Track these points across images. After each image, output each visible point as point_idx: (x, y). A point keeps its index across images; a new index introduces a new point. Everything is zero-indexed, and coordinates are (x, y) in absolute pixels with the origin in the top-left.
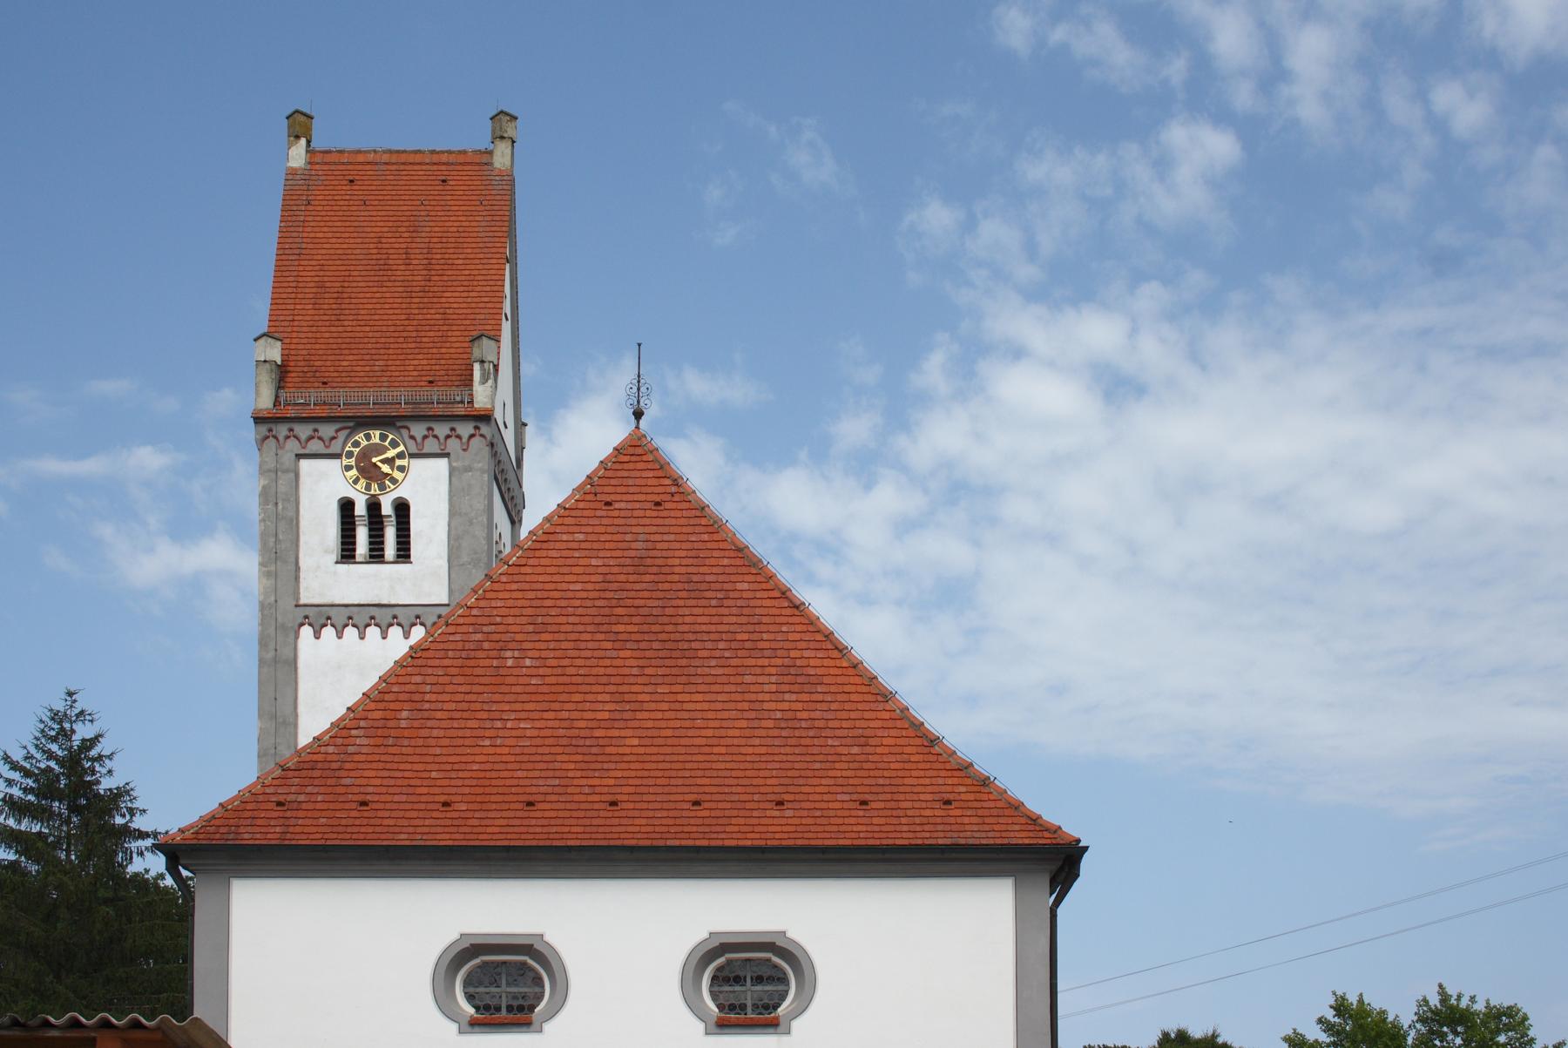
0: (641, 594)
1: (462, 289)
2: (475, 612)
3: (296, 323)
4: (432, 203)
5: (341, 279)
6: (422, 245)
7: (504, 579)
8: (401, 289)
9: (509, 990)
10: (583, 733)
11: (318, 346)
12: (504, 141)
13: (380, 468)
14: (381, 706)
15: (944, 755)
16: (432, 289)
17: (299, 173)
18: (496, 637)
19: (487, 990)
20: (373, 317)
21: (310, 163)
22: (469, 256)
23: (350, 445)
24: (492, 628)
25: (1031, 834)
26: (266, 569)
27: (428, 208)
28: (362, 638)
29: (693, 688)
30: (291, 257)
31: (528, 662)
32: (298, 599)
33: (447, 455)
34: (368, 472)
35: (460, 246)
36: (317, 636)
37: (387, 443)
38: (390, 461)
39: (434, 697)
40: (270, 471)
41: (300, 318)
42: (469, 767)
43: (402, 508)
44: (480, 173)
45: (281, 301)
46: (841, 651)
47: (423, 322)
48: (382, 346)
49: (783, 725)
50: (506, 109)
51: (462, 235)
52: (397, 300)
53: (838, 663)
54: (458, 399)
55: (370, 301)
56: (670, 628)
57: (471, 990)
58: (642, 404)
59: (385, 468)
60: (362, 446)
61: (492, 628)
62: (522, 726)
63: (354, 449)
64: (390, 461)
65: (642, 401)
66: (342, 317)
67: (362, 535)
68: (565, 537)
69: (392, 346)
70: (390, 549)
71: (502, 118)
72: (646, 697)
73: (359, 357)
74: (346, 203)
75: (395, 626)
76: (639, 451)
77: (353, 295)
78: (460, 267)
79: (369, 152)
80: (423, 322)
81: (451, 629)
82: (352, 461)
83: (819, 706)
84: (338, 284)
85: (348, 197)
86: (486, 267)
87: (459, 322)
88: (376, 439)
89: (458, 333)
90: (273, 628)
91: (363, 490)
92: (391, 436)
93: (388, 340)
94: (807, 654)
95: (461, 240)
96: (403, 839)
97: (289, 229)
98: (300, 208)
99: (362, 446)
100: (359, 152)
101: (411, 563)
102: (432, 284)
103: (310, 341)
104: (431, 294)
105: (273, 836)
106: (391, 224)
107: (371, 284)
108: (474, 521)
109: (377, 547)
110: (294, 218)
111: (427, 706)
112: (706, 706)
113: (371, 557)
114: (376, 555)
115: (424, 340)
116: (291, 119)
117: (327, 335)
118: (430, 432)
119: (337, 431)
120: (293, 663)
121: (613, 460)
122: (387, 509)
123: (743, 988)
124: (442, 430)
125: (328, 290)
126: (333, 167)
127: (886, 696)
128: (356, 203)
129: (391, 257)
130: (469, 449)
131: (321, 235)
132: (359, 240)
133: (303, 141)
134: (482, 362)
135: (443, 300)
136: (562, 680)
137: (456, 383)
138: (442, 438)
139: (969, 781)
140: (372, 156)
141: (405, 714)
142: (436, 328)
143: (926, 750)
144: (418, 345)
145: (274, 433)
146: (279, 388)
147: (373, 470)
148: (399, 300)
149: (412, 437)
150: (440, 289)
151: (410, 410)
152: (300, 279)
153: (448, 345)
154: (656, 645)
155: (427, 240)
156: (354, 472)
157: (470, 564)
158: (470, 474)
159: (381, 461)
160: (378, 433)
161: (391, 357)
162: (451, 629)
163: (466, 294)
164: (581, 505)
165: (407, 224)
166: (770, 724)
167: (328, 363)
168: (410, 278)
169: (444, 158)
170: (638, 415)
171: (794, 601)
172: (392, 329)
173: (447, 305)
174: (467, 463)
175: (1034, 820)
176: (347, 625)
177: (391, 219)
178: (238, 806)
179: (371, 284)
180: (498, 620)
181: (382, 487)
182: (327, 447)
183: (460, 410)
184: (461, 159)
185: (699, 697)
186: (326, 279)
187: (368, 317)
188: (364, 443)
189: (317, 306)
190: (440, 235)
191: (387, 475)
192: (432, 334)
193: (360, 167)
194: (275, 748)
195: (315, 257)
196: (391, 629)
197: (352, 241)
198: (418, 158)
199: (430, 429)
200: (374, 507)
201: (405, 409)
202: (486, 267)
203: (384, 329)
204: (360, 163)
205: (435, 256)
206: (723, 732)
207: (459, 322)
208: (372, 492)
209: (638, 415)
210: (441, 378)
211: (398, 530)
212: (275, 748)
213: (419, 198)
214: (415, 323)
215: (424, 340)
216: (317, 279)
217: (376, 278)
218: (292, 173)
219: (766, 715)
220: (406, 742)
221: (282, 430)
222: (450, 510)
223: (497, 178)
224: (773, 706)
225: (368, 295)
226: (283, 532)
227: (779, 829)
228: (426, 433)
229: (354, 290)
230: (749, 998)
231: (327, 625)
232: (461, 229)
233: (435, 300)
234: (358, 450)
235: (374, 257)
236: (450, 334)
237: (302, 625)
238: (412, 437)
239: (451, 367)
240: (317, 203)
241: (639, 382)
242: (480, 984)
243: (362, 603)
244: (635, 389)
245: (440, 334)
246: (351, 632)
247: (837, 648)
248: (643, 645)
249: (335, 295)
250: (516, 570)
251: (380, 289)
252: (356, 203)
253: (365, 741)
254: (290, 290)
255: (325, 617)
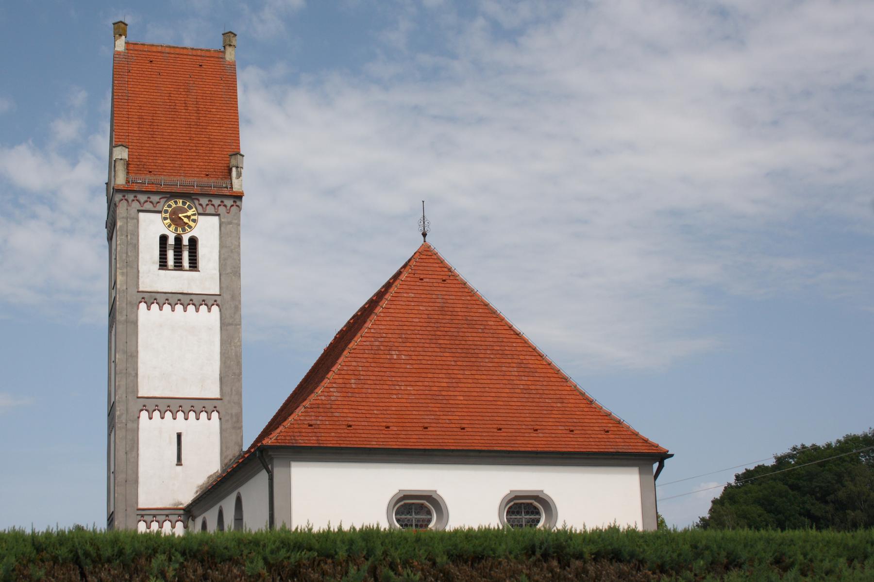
0: (446, 325)
1: (217, 125)
2: (372, 331)
3: (130, 137)
4: (196, 77)
5: (151, 115)
6: (193, 100)
7: (382, 315)
8: (184, 123)
9: (416, 517)
10: (437, 393)
11: (143, 151)
12: (231, 47)
13: (183, 220)
14: (341, 376)
15: (598, 408)
16: (201, 124)
17: (122, 54)
18: (386, 344)
19: (405, 517)
20: (171, 137)
21: (127, 49)
22: (218, 107)
23: (166, 206)
24: (382, 339)
25: (647, 448)
26: (121, 271)
27: (194, 79)
28: (173, 311)
29: (480, 373)
30: (123, 101)
31: (403, 357)
32: (138, 288)
33: (218, 215)
34: (176, 221)
35: (213, 101)
36: (149, 308)
37: (186, 207)
38: (188, 217)
39: (364, 373)
40: (123, 218)
41: (132, 134)
42: (390, 408)
43: (193, 241)
44: (219, 63)
45: (121, 125)
46: (541, 357)
47: (199, 142)
48: (178, 153)
49: (525, 392)
50: (232, 31)
51: (214, 95)
52: (183, 129)
53: (541, 362)
54: (224, 186)
55: (169, 128)
56: (463, 342)
57: (399, 517)
58: (426, 230)
59: (186, 220)
60: (173, 207)
61: (382, 339)
62: (409, 389)
63: (168, 209)
64: (188, 217)
65: (426, 229)
66: (155, 136)
67: (171, 255)
68: (405, 295)
69: (183, 154)
70: (186, 263)
71: (229, 36)
72: (461, 376)
73: (166, 159)
74: (149, 73)
75: (204, 305)
76: (429, 253)
77: (159, 124)
78: (214, 113)
79: (158, 46)
80: (199, 142)
81: (364, 339)
82: (168, 215)
83: (538, 383)
84: (150, 118)
85: (150, 70)
86: (228, 114)
87: (217, 143)
88: (180, 204)
89: (218, 149)
90: (125, 303)
91: (173, 231)
92: (188, 203)
93: (181, 150)
94: (527, 357)
95: (213, 98)
96: (374, 444)
97: (120, 85)
98: (124, 74)
99: (173, 207)
100: (153, 45)
101: (199, 271)
102: (201, 121)
103: (139, 148)
104: (201, 127)
105: (312, 442)
106: (175, 87)
107: (168, 119)
108: (233, 251)
109: (178, 261)
110: (122, 79)
111: (362, 377)
112: (489, 381)
113: (175, 266)
114: (178, 266)
115: (200, 151)
116: (116, 25)
117: (148, 145)
118: (210, 202)
119: (160, 199)
120: (135, 323)
121: (419, 257)
122: (185, 242)
123: (521, 517)
124: (216, 202)
125: (145, 120)
126: (140, 53)
127: (565, 379)
128: (155, 73)
129: (177, 104)
130: (231, 212)
131: (137, 89)
132: (159, 94)
133: (123, 37)
134: (237, 167)
135: (207, 130)
136: (421, 366)
137: (221, 176)
138: (216, 206)
139: (612, 421)
140: (160, 48)
141: (353, 381)
142: (206, 145)
143: (589, 406)
144: (197, 154)
145: (126, 197)
146: (128, 173)
147: (179, 220)
148: (184, 129)
149: (201, 205)
150: (205, 124)
151: (199, 190)
152: (130, 113)
153: (213, 155)
154: (459, 351)
155: (195, 97)
156: (168, 221)
157: (231, 274)
158: (231, 225)
159: (184, 216)
160: (181, 201)
161: (184, 160)
162: (364, 339)
163: (219, 128)
164: (409, 279)
165: (183, 87)
166: (519, 391)
167: (150, 161)
168: (189, 117)
169: (199, 53)
170: (424, 235)
171: (516, 331)
172: (182, 144)
173: (210, 133)
174: (229, 220)
175: (646, 441)
176: (165, 303)
177: (175, 84)
178: (290, 426)
179: (168, 119)
180: (384, 335)
181: (184, 230)
182: (155, 207)
183: (226, 192)
184: (208, 54)
185: (484, 377)
186: (143, 114)
187: (168, 137)
188: (174, 206)
189: (140, 129)
190: (201, 95)
191: (187, 223)
192: (204, 148)
193: (154, 54)
194: (126, 370)
195: (136, 102)
196: (189, 307)
197: (155, 94)
198: (185, 52)
199: (211, 201)
200: (178, 240)
201: (196, 190)
202: (228, 114)
203: (178, 144)
204: (154, 52)
205: (200, 106)
206: (499, 395)
207: (217, 143)
208: (178, 232)
209: (424, 235)
210: (212, 173)
211: (189, 252)
212: (126, 370)
213: (189, 73)
214: (194, 142)
215: (200, 151)
216: (138, 114)
217: (171, 116)
218: (117, 55)
219: (516, 386)
220: (357, 395)
221: (131, 197)
222: (220, 244)
223: (228, 66)
224: (518, 382)
225: (167, 125)
226: (131, 251)
227: (539, 442)
228: (208, 203)
229: (160, 121)
230: (524, 521)
231: (142, 302)
232: (212, 92)
233: (203, 130)
234: (170, 209)
235: (168, 104)
236: (213, 149)
237: (141, 302)
238: (201, 205)
239: (216, 167)
240: (133, 71)
241: (424, 219)
242: (403, 513)
243: (173, 291)
244: (422, 223)
245: (208, 149)
246: (167, 307)
247: (540, 355)
248: (454, 350)
249: (150, 123)
250: (387, 310)
251: (173, 122)
252: (155, 73)
253: (339, 394)
254: (124, 119)
255: (153, 298)
